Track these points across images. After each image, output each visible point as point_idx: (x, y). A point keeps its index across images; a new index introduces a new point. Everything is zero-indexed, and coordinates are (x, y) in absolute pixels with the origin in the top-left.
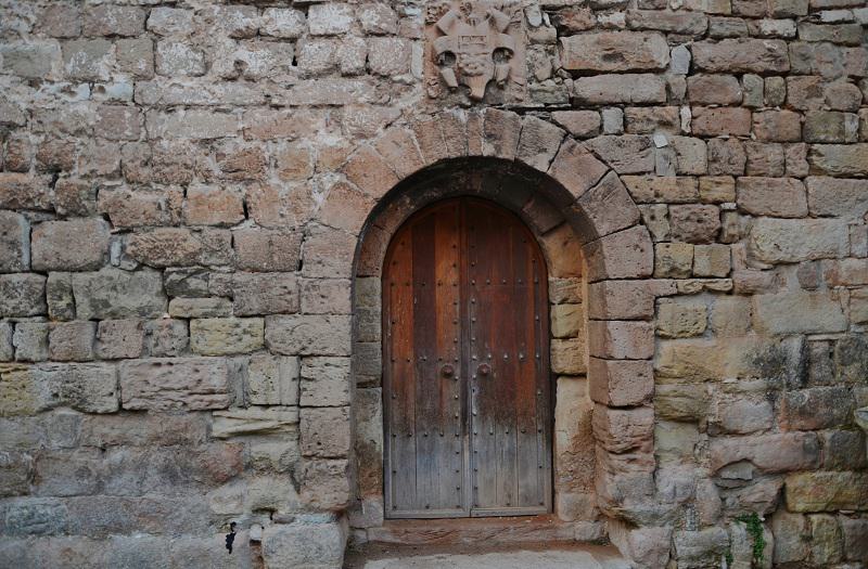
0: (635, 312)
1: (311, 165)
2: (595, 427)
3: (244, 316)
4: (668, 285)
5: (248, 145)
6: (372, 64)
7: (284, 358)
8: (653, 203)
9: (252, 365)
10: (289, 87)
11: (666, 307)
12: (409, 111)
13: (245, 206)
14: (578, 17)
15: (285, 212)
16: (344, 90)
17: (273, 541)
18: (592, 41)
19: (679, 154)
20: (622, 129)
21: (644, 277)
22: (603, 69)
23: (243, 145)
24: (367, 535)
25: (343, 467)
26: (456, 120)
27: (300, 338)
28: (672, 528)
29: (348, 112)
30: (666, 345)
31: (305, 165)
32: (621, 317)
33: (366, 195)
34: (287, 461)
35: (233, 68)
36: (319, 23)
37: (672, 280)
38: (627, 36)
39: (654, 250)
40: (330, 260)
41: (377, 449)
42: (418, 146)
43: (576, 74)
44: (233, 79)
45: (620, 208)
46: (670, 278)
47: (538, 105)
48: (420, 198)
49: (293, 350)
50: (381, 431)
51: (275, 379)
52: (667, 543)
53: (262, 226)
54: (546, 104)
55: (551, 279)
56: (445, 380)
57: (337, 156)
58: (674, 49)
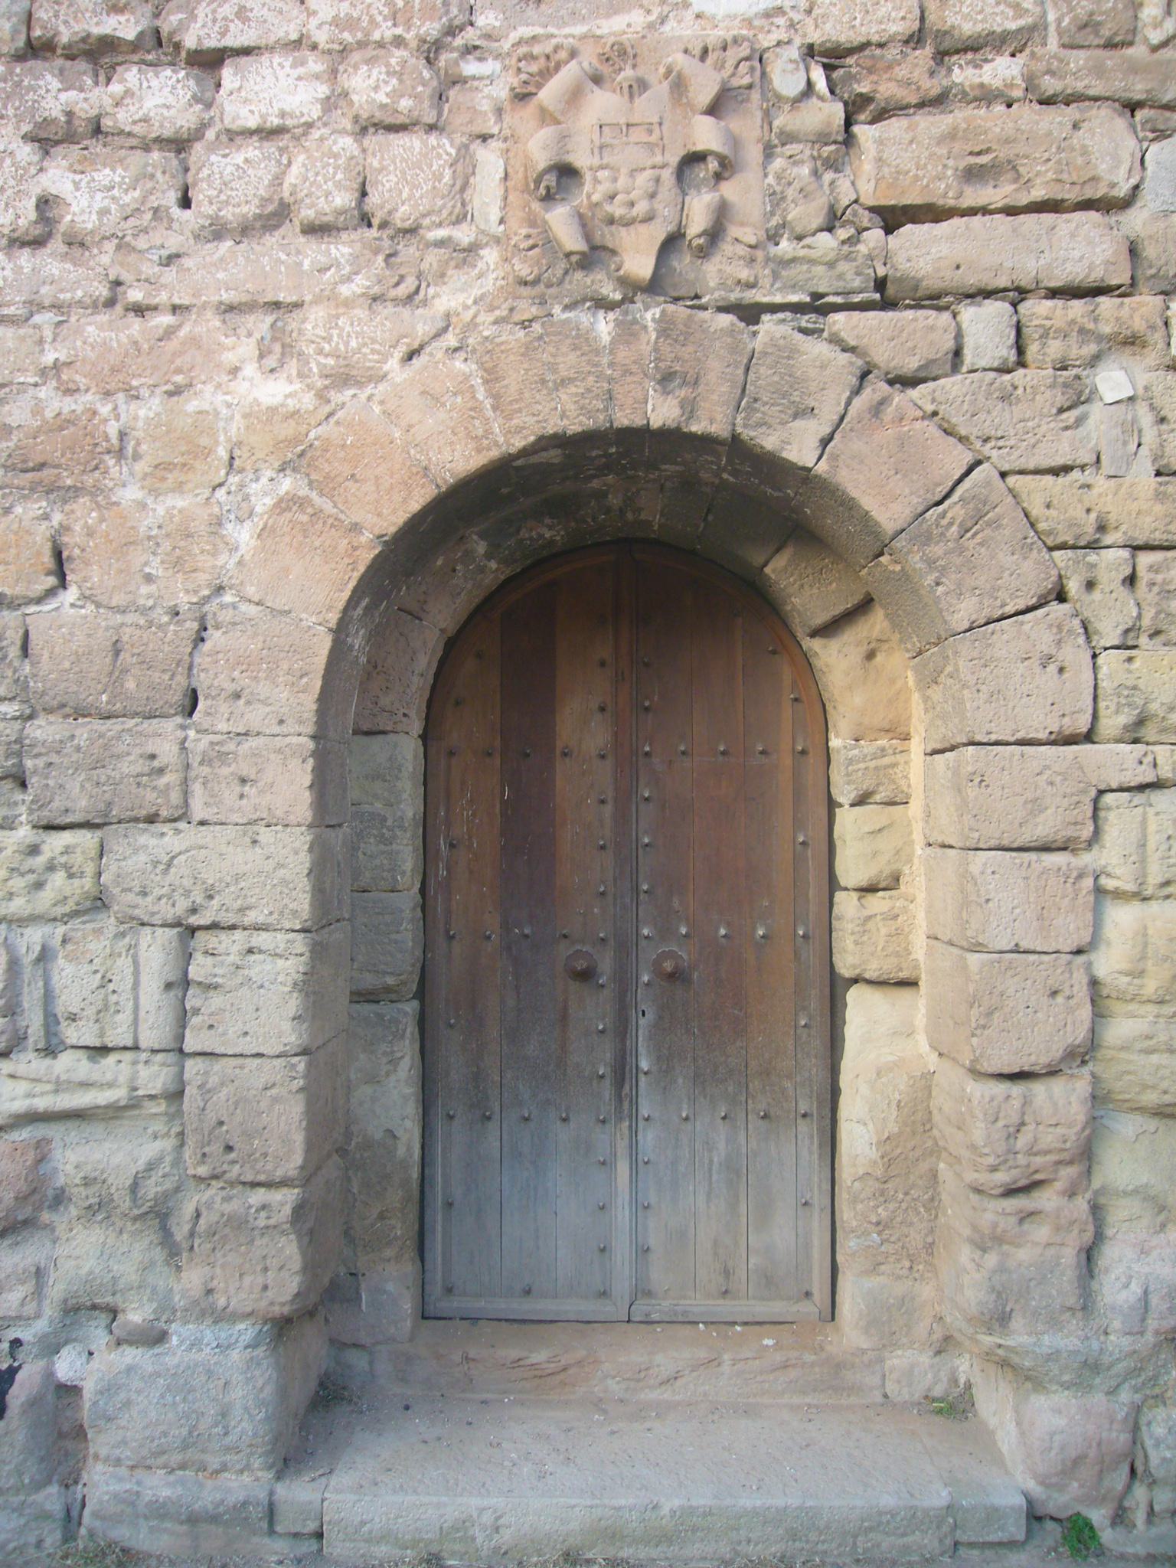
0: (1044, 828)
1: (222, 453)
2: (937, 1117)
3: (50, 827)
4: (1130, 762)
5: (68, 405)
6: (374, 199)
7: (148, 930)
8: (1093, 546)
9: (69, 947)
10: (170, 260)
11: (1120, 814)
12: (467, 316)
13: (58, 555)
14: (901, 72)
15: (155, 568)
16: (307, 264)
17: (108, 1390)
18: (936, 131)
19: (1163, 420)
20: (1013, 357)
21: (1070, 740)
22: (966, 202)
23: (55, 404)
24: (371, 1363)
25: (287, 1210)
26: (583, 341)
27: (187, 883)
28: (1138, 1397)
29: (313, 321)
30: (1121, 918)
31: (208, 452)
32: (1005, 843)
33: (356, 528)
34: (152, 1189)
35: (33, 215)
36: (246, 101)
37: (1140, 748)
38: (1028, 115)
39: (1095, 668)
40: (263, 689)
41: (401, 1152)
42: (488, 404)
43: (892, 218)
44: (37, 243)
45: (1007, 559)
46: (1136, 741)
47: (794, 298)
48: (512, 542)
49: (169, 913)
50: (412, 1109)
51: (122, 980)
52: (1124, 1438)
53: (98, 605)
54: (817, 296)
55: (835, 743)
56: (574, 986)
57: (288, 430)
58: (1154, 148)
